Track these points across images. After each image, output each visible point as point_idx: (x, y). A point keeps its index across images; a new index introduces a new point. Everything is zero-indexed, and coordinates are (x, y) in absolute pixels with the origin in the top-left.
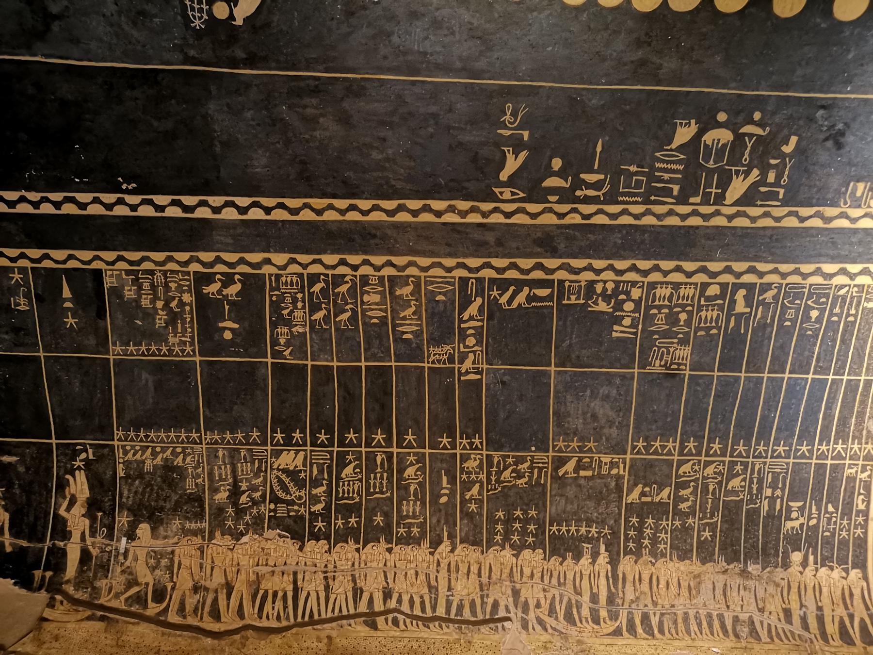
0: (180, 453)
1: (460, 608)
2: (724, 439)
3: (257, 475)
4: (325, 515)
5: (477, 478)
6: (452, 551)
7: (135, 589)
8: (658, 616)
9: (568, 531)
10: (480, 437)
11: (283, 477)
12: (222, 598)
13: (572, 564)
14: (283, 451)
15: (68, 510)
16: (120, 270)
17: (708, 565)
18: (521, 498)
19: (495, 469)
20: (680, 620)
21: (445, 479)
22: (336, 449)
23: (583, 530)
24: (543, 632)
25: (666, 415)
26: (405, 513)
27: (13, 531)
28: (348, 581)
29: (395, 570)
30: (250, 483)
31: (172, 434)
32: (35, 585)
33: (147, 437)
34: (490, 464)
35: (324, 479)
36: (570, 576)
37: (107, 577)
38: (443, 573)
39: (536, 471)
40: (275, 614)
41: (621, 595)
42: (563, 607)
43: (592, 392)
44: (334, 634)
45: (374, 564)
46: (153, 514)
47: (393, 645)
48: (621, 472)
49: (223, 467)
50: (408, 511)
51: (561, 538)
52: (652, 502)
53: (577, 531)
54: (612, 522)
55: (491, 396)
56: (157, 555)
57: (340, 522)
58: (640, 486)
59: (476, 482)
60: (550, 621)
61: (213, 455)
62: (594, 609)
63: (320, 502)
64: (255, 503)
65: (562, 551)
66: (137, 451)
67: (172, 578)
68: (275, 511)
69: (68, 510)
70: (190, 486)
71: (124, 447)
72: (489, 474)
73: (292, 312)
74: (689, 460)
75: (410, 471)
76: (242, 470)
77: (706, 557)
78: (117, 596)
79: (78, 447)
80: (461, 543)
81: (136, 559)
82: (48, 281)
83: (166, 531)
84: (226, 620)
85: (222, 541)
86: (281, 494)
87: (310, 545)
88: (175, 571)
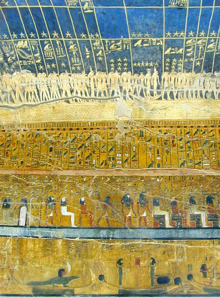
1: (100, 94)
2: (206, 31)
3: (11, 51)
6: (95, 74)
8: (176, 92)
9: (141, 65)
10: (98, 34)
11: (22, 50)
14: (18, 41)
17: (198, 74)
18: (120, 55)
20: (185, 93)
21: (87, 49)
25: (179, 23)
34: (104, 43)
36: (142, 80)
39: (124, 45)
41: (162, 85)
43: (145, 16)
44: (55, 105)
45: (65, 80)
48: (161, 44)
51: (138, 67)
52: (175, 54)
53: (145, 65)
54: (159, 61)
55: (100, 19)
58: (170, 48)
60: (134, 96)
64: (14, 61)
68: (22, 63)
72: (105, 47)
74: (190, 39)
75: (72, 47)
77: (198, 70)
86: (22, 57)
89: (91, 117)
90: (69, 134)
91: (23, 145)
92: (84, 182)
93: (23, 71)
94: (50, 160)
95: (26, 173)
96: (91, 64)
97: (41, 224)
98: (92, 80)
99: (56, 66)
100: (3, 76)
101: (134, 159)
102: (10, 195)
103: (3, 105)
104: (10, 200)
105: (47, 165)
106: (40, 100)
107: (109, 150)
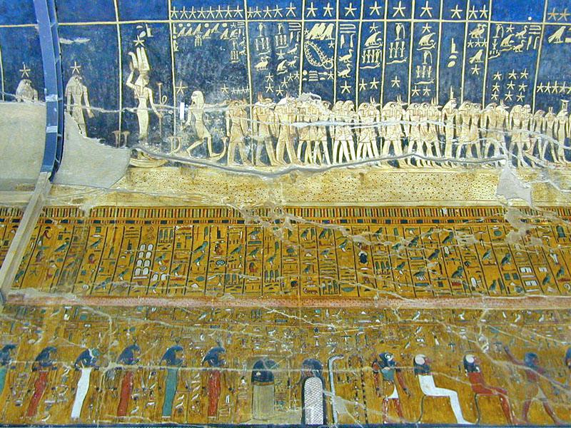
0: (225, 28)
3: (292, 46)
4: (351, 80)
5: (481, 44)
6: (457, 107)
7: (198, 143)
9: (551, 90)
10: (487, 8)
13: (551, 116)
15: (133, 81)
19: (497, 37)
21: (454, 46)
22: (361, 20)
23: (563, 88)
24: (529, 167)
26: (418, 76)
27: (92, 101)
28: (372, 132)
29: (410, 123)
30: (286, 53)
31: (219, 11)
32: (117, 143)
33: (197, 14)
35: (350, 48)
36: (550, 126)
38: (450, 126)
39: (530, 38)
40: (315, 159)
42: (544, 149)
44: (365, 171)
45: (393, 118)
46: (204, 82)
47: (413, 179)
49: (263, 39)
50: (421, 75)
51: (545, 95)
56: (212, 116)
57: (363, 85)
59: (480, 48)
60: (534, 159)
61: (253, 28)
62: (567, 150)
63: (346, 68)
64: (290, 70)
65: (545, 106)
68: (307, 76)
69: (133, 81)
70: (234, 58)
71: (177, 25)
72: (491, 41)
75: (425, 39)
76: (279, 42)
78: (184, 148)
79: (139, 27)
80: (464, 100)
81: (194, 120)
83: (216, 97)
84: (275, 164)
85: (263, 105)
86: (312, 62)
87: (338, 105)
88: (228, 128)
89: (447, 198)
90: (400, 231)
91: (290, 250)
92: (464, 323)
93: (303, 96)
94: (365, 278)
95: (308, 304)
96: (453, 83)
97: (369, 418)
98: (450, 119)
99: (379, 85)
100: (258, 103)
101: (561, 276)
102: (270, 353)
103: (243, 168)
104: (270, 364)
105: (359, 288)
106: (332, 162)
107: (500, 261)
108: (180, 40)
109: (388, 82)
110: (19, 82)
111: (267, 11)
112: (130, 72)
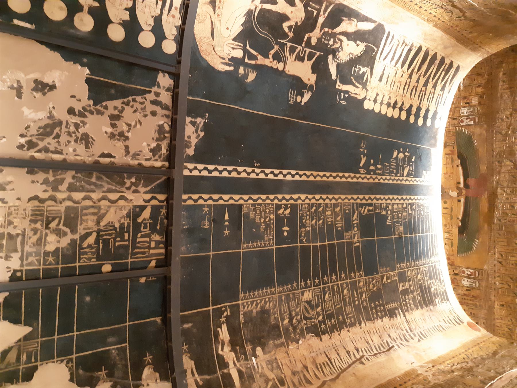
3: (297, 307)
12: (306, 373)
15: (222, 350)
16: (249, 204)
37: (255, 381)
66: (249, 304)
67: (281, 371)
69: (222, 350)
70: (273, 321)
73: (306, 221)
75: (345, 292)
81: (262, 368)
82: (219, 210)
83: (268, 349)
85: (292, 347)
87: (323, 337)
108: (245, 314)
109: (338, 319)
110: (143, 369)
111: (285, 287)
112: (219, 343)
